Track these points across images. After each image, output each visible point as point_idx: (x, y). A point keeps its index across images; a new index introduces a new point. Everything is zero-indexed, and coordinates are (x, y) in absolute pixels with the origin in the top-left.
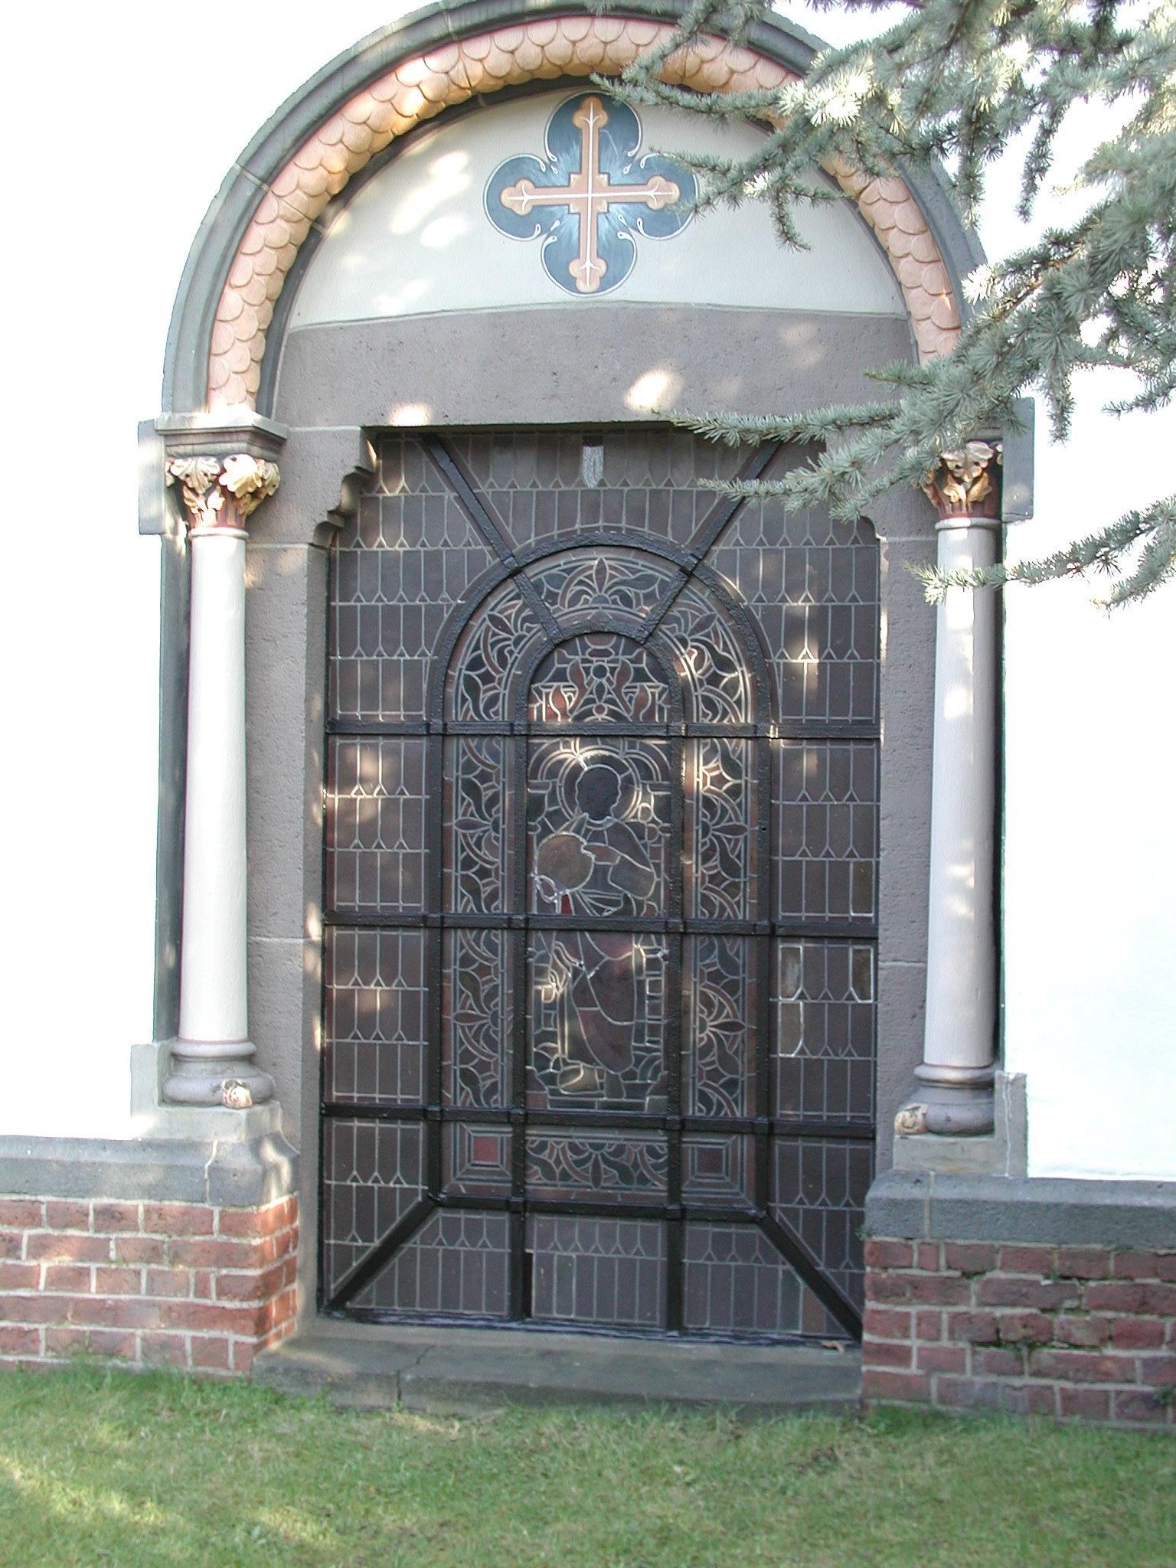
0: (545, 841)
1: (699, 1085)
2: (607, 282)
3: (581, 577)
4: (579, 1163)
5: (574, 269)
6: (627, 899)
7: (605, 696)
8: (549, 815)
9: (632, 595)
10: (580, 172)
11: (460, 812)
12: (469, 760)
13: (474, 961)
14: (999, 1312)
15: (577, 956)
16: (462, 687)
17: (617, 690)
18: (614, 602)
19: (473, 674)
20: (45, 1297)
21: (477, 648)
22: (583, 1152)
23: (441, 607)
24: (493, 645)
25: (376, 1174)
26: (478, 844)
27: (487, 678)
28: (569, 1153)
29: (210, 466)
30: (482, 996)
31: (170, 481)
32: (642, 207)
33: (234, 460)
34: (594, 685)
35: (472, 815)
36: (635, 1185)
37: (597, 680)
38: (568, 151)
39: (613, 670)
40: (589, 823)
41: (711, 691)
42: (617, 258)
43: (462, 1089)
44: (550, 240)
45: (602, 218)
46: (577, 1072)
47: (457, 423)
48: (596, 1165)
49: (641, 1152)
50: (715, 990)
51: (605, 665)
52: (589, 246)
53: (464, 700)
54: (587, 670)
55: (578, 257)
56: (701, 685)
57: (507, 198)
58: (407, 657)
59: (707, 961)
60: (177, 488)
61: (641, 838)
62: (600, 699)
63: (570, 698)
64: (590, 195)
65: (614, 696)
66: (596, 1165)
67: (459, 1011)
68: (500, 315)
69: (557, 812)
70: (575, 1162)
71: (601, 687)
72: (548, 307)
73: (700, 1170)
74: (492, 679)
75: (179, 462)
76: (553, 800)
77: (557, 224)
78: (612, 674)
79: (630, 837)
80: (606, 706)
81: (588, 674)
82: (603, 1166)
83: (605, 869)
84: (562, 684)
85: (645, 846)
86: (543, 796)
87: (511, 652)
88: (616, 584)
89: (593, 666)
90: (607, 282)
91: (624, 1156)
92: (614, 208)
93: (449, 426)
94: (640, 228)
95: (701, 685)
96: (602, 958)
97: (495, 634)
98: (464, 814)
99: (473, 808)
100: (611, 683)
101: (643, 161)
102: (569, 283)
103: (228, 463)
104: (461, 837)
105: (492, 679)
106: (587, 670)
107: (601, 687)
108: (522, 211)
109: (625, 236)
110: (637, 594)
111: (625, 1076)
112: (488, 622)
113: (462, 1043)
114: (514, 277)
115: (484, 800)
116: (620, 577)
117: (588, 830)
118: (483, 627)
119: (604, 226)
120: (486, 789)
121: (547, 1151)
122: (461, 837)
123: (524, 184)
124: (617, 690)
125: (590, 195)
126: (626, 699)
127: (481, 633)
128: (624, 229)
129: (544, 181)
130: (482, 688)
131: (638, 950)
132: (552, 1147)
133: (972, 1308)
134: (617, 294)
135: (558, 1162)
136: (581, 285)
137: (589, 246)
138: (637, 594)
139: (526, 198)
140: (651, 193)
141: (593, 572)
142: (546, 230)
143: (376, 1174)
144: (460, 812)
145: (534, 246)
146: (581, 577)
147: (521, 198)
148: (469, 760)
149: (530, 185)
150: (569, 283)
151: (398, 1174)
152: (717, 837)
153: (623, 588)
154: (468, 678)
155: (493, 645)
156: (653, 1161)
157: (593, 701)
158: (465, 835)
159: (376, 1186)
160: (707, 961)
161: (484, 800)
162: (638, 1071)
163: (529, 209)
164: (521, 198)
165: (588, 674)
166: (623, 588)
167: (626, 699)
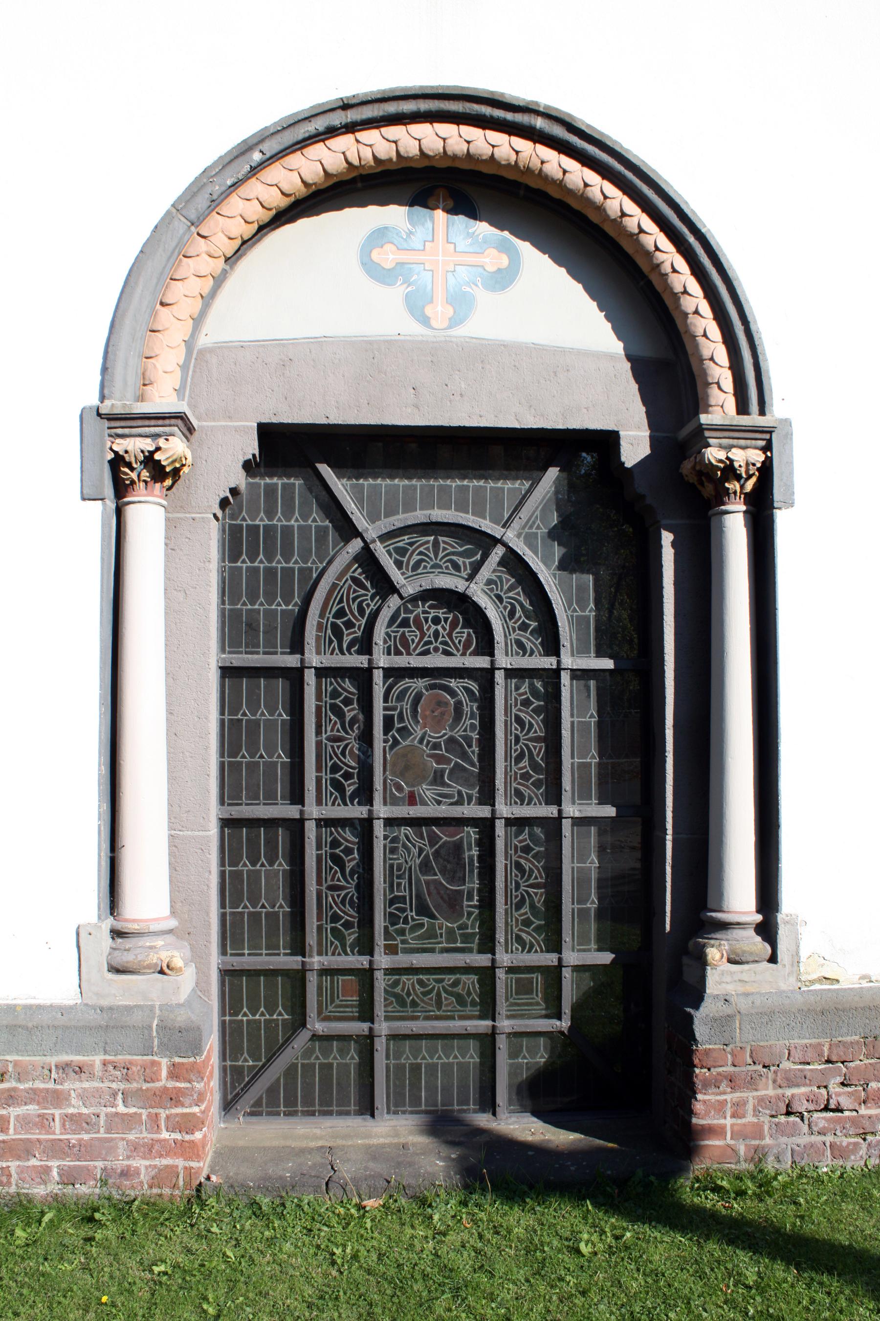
0: (395, 750)
1: (515, 930)
2: (454, 322)
3: (421, 549)
4: (425, 994)
5: (428, 311)
6: (460, 793)
7: (440, 639)
8: (399, 730)
9: (461, 563)
10: (433, 241)
11: (329, 729)
12: (335, 689)
13: (341, 844)
14: (789, 1092)
15: (422, 838)
16: (329, 631)
17: (450, 635)
18: (447, 568)
19: (338, 622)
20: (13, 1140)
21: (341, 601)
22: (428, 986)
23: (311, 569)
24: (354, 599)
25: (262, 1009)
26: (343, 753)
27: (349, 625)
28: (417, 987)
29: (148, 445)
30: (348, 870)
31: (111, 456)
32: (480, 270)
33: (167, 440)
34: (432, 631)
35: (338, 731)
36: (469, 1008)
37: (434, 627)
38: (423, 225)
39: (446, 619)
40: (430, 736)
41: (521, 636)
42: (461, 304)
43: (332, 943)
44: (409, 289)
45: (450, 275)
46: (422, 925)
47: (336, 422)
48: (439, 995)
49: (413, 984)
50: (526, 859)
51: (440, 615)
52: (440, 296)
53: (331, 642)
54: (426, 619)
55: (432, 302)
56: (514, 631)
57: (375, 255)
58: (284, 607)
59: (521, 838)
60: (118, 462)
61: (470, 746)
62: (436, 642)
63: (413, 641)
64: (440, 258)
65: (447, 639)
66: (439, 995)
67: (330, 883)
68: (370, 343)
69: (405, 728)
70: (422, 993)
71: (436, 634)
72: (408, 338)
73: (516, 994)
74: (353, 626)
75: (118, 441)
76: (401, 718)
77: (415, 277)
78: (446, 622)
79: (461, 745)
80: (441, 646)
81: (427, 621)
82: (444, 995)
83: (443, 771)
84: (406, 630)
85: (473, 752)
86: (393, 716)
87: (368, 605)
88: (453, 554)
89: (431, 616)
90: (454, 322)
91: (460, 986)
92: (458, 268)
93: (329, 425)
94: (479, 284)
95: (514, 631)
96: (441, 838)
97: (355, 591)
98: (332, 730)
99: (338, 725)
100: (444, 629)
101: (481, 236)
102: (425, 321)
103: (161, 442)
104: (329, 748)
105: (353, 626)
106: (426, 619)
107: (436, 634)
108: (388, 265)
109: (468, 289)
110: (464, 563)
111: (460, 928)
112: (350, 582)
113: (331, 908)
114: (381, 315)
115: (348, 719)
116: (451, 550)
117: (429, 742)
118: (346, 586)
119: (452, 281)
120: (349, 711)
121: (401, 986)
122: (329, 748)
123: (388, 247)
124: (450, 635)
125: (440, 258)
126: (457, 642)
127: (345, 590)
128: (468, 284)
129: (405, 246)
130: (346, 632)
131: (468, 832)
132: (404, 983)
133: (771, 1092)
134: (463, 331)
135: (409, 994)
136: (434, 323)
137: (440, 296)
138: (464, 563)
139: (391, 257)
140: (487, 260)
141: (430, 545)
142: (407, 282)
143: (262, 1009)
144: (329, 729)
145: (397, 293)
146: (421, 549)
147: (387, 257)
148: (335, 689)
149: (394, 248)
150: (425, 321)
151: (245, 1009)
152: (527, 746)
153: (452, 557)
154: (334, 625)
155: (354, 599)
156: (422, 989)
157: (430, 643)
158: (332, 747)
159: (263, 1018)
160: (521, 838)
161: (348, 719)
162: (470, 923)
163: (393, 265)
164: (387, 257)
165: (427, 621)
166: (452, 557)
167: (457, 642)
